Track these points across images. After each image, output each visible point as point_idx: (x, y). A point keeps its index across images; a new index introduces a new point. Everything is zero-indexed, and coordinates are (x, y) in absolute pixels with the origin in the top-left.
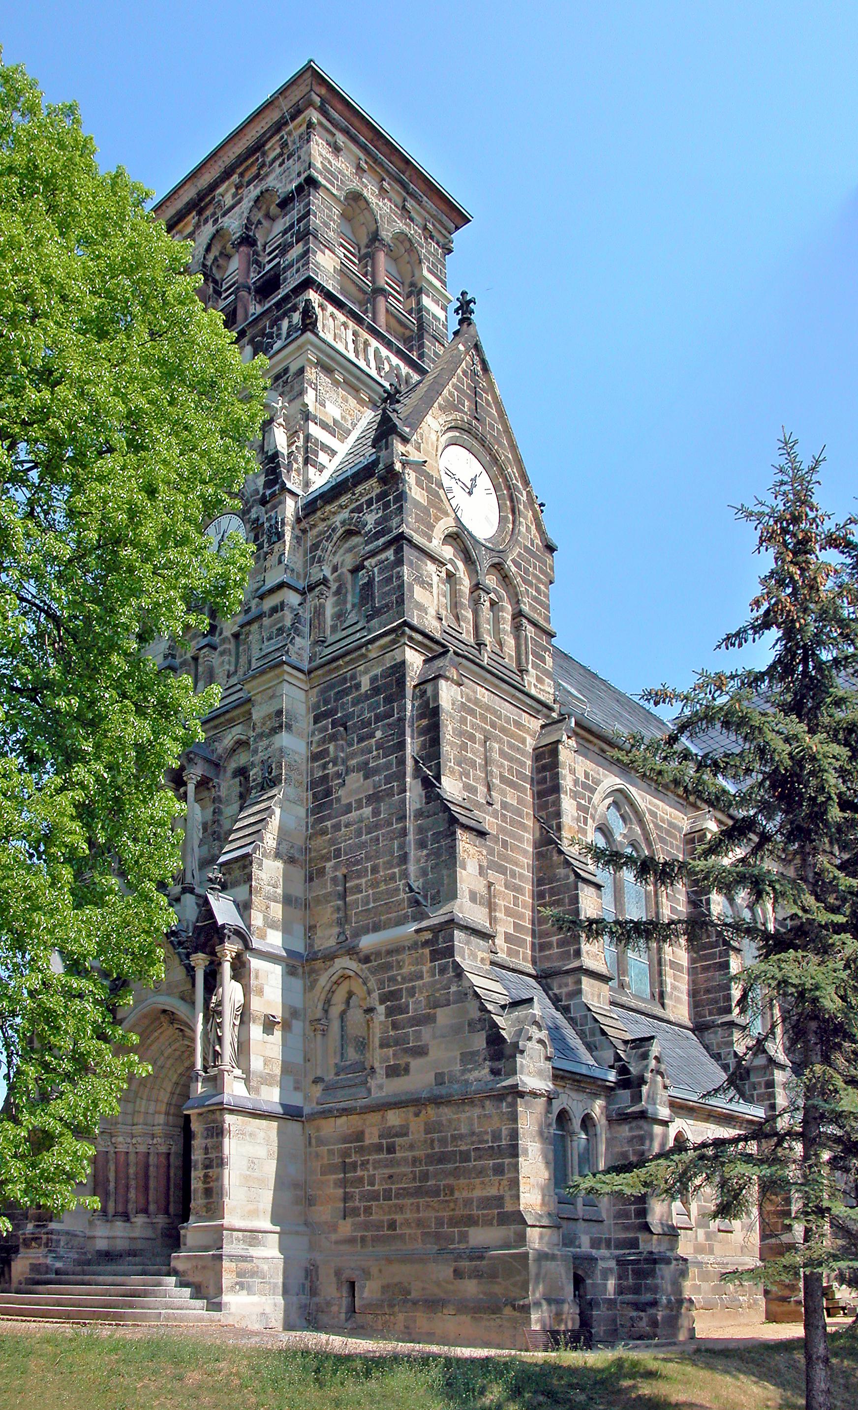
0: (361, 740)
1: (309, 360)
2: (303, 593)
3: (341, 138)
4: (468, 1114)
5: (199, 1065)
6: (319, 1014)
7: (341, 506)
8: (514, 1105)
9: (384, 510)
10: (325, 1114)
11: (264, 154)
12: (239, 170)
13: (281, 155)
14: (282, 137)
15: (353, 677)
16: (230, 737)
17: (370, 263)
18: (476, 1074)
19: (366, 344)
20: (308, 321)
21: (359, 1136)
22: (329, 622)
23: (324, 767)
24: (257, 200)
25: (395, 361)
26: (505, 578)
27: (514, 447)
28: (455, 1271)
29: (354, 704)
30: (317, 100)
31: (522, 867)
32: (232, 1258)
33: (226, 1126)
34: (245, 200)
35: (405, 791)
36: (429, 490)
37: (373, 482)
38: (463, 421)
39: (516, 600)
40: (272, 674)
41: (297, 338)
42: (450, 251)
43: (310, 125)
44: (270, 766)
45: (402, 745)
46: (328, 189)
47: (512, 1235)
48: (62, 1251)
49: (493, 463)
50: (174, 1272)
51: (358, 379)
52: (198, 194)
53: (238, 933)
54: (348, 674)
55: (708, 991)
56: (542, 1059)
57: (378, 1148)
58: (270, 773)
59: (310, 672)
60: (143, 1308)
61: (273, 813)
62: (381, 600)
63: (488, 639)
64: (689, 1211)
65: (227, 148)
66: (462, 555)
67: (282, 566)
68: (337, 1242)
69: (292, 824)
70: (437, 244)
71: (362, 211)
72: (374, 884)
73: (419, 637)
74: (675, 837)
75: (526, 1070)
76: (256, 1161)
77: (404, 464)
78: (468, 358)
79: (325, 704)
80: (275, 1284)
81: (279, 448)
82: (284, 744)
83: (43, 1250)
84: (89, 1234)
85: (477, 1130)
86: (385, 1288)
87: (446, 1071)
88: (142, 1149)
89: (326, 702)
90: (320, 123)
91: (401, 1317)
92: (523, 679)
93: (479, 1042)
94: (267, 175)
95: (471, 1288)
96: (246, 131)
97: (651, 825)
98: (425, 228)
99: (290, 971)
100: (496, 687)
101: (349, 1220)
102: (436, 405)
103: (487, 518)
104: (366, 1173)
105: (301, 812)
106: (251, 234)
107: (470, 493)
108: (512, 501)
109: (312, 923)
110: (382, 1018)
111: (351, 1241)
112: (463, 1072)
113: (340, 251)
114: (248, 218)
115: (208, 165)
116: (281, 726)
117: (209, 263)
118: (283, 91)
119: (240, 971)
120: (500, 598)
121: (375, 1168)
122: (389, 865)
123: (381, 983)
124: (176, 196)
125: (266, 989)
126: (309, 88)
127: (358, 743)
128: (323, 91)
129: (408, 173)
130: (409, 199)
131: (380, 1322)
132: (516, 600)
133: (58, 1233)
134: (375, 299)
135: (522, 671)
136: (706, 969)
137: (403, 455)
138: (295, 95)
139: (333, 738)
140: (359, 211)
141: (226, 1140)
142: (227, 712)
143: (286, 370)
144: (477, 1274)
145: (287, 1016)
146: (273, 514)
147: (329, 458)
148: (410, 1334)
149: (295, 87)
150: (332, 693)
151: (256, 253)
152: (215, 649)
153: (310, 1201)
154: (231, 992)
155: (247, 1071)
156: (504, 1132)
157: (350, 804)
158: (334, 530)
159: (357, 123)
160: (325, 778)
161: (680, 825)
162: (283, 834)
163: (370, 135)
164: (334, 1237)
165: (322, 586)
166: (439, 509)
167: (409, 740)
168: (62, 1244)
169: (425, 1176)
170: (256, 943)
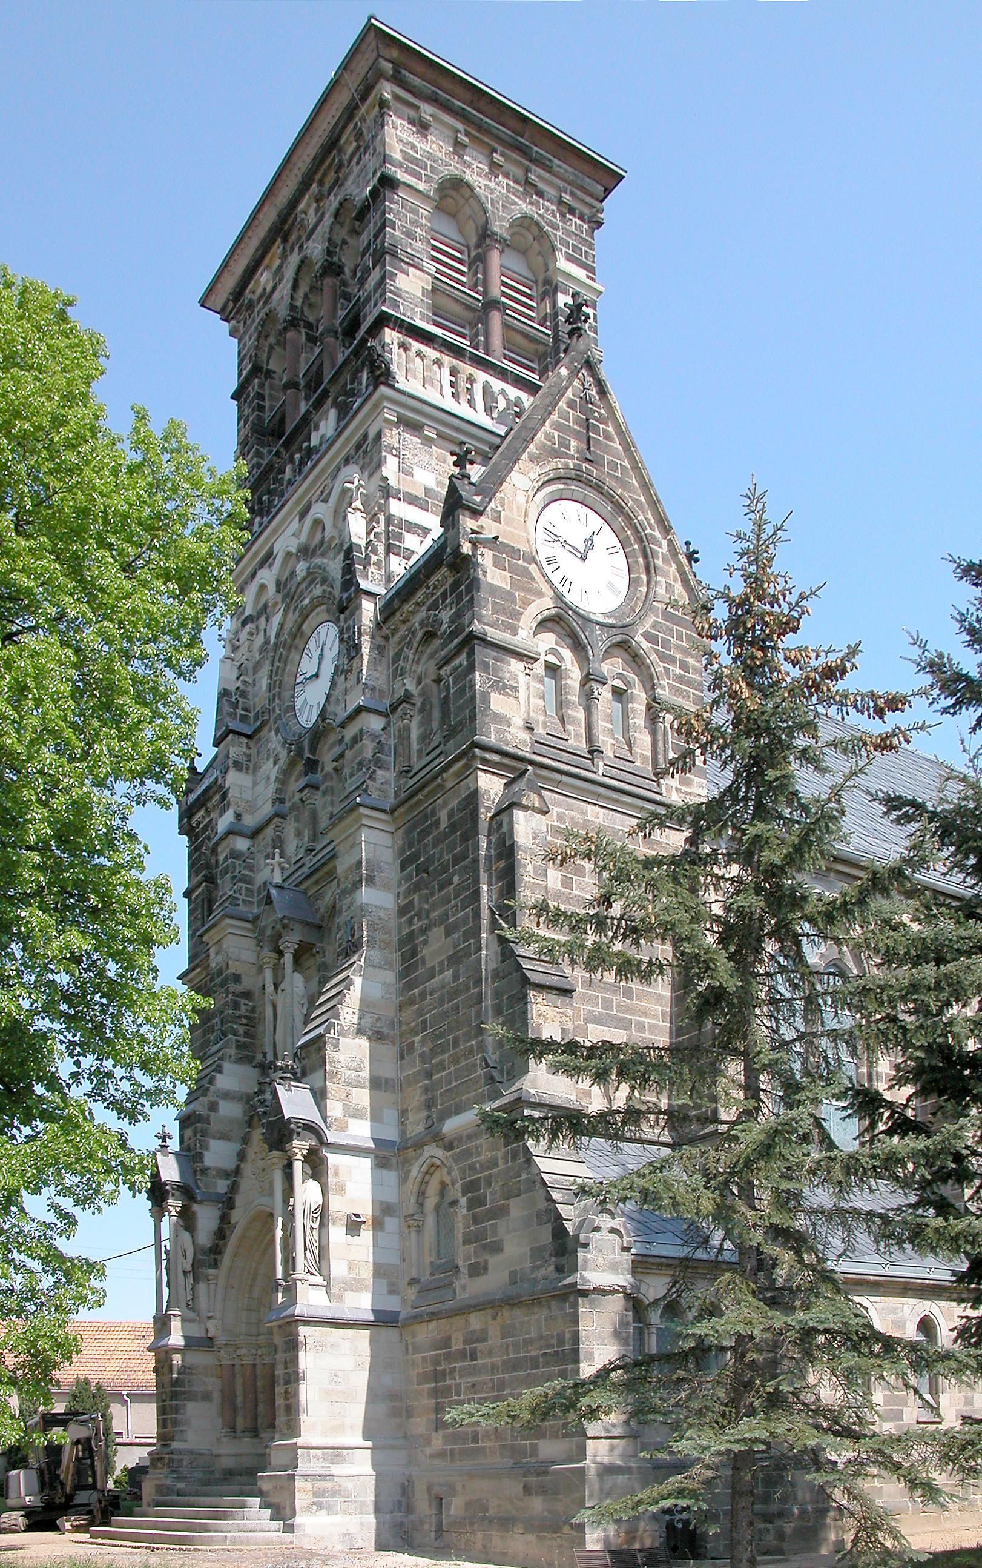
0: (441, 888)
1: (387, 420)
2: (387, 716)
3: (427, 110)
4: (537, 1316)
5: (279, 1276)
6: (412, 1208)
7: (417, 604)
8: (575, 1305)
9: (458, 604)
10: (417, 1319)
11: (341, 151)
12: (317, 177)
13: (358, 148)
14: (356, 124)
15: (433, 813)
16: (330, 893)
17: (481, 269)
18: (543, 1271)
19: (471, 379)
20: (378, 373)
21: (446, 1342)
23: (410, 922)
24: (337, 215)
25: (514, 393)
26: (635, 659)
27: (646, 486)
28: (525, 1487)
29: (434, 847)
30: (388, 67)
31: (655, 1017)
32: (306, 1477)
33: (301, 1338)
34: (327, 216)
35: (480, 949)
36: (514, 569)
37: (444, 570)
38: (567, 467)
39: (650, 685)
40: (349, 819)
41: (370, 395)
42: (599, 224)
43: (383, 104)
44: (352, 928)
45: (477, 893)
46: (409, 186)
47: (574, 1447)
48: (185, 1471)
49: (618, 514)
50: (260, 1493)
51: (458, 430)
52: (279, 216)
53: (310, 1128)
54: (429, 810)
56: (617, 1249)
57: (462, 1355)
58: (353, 936)
59: (393, 811)
60: (216, 1531)
61: (351, 983)
62: (456, 717)
63: (607, 742)
65: (299, 151)
66: (569, 641)
67: (361, 686)
68: (432, 1456)
69: (377, 992)
70: (581, 218)
71: (467, 200)
72: (455, 1060)
73: (496, 758)
75: (591, 1265)
76: (340, 1374)
77: (475, 544)
78: (576, 383)
79: (410, 847)
80: (363, 1503)
81: (354, 540)
82: (364, 901)
83: (166, 1470)
84: (215, 1452)
85: (544, 1334)
86: (468, 1505)
87: (518, 1268)
88: (248, 1360)
89: (410, 846)
90: (396, 97)
91: (480, 1535)
92: (659, 785)
93: (545, 1235)
94: (345, 179)
95: (537, 1505)
96: (316, 124)
99: (381, 1162)
100: (616, 801)
101: (440, 1432)
102: (525, 456)
103: (610, 585)
104: (453, 1381)
105: (390, 976)
106: (335, 259)
107: (583, 559)
108: (645, 557)
109: (405, 1106)
110: (465, 1211)
111: (442, 1454)
112: (534, 1269)
113: (431, 267)
114: (329, 240)
115: (284, 177)
116: (361, 881)
117: (298, 303)
118: (346, 65)
119: (316, 1167)
120: (628, 684)
121: (461, 1377)
122: (468, 1037)
123: (463, 1171)
124: (256, 222)
125: (349, 1187)
126: (375, 54)
127: (439, 891)
128: (395, 53)
129: (527, 134)
130: (533, 167)
131: (463, 1541)
132: (650, 684)
133: (180, 1452)
134: (487, 316)
137: (473, 532)
138: (362, 67)
139: (417, 887)
140: (462, 201)
141: (302, 1354)
142: (324, 864)
143: (365, 436)
144: (543, 1491)
145: (378, 1213)
146: (351, 622)
147: (419, 539)
148: (487, 1553)
149: (359, 56)
150: (415, 834)
151: (344, 283)
152: (318, 788)
153: (409, 1413)
154: (307, 1193)
155: (328, 1279)
156: (568, 1336)
157: (433, 967)
158: (414, 633)
159: (448, 85)
160: (411, 935)
162: (366, 1005)
163: (468, 96)
164: (428, 1451)
165: (404, 705)
166: (529, 590)
167: (485, 888)
168: (185, 1463)
170: (331, 1137)
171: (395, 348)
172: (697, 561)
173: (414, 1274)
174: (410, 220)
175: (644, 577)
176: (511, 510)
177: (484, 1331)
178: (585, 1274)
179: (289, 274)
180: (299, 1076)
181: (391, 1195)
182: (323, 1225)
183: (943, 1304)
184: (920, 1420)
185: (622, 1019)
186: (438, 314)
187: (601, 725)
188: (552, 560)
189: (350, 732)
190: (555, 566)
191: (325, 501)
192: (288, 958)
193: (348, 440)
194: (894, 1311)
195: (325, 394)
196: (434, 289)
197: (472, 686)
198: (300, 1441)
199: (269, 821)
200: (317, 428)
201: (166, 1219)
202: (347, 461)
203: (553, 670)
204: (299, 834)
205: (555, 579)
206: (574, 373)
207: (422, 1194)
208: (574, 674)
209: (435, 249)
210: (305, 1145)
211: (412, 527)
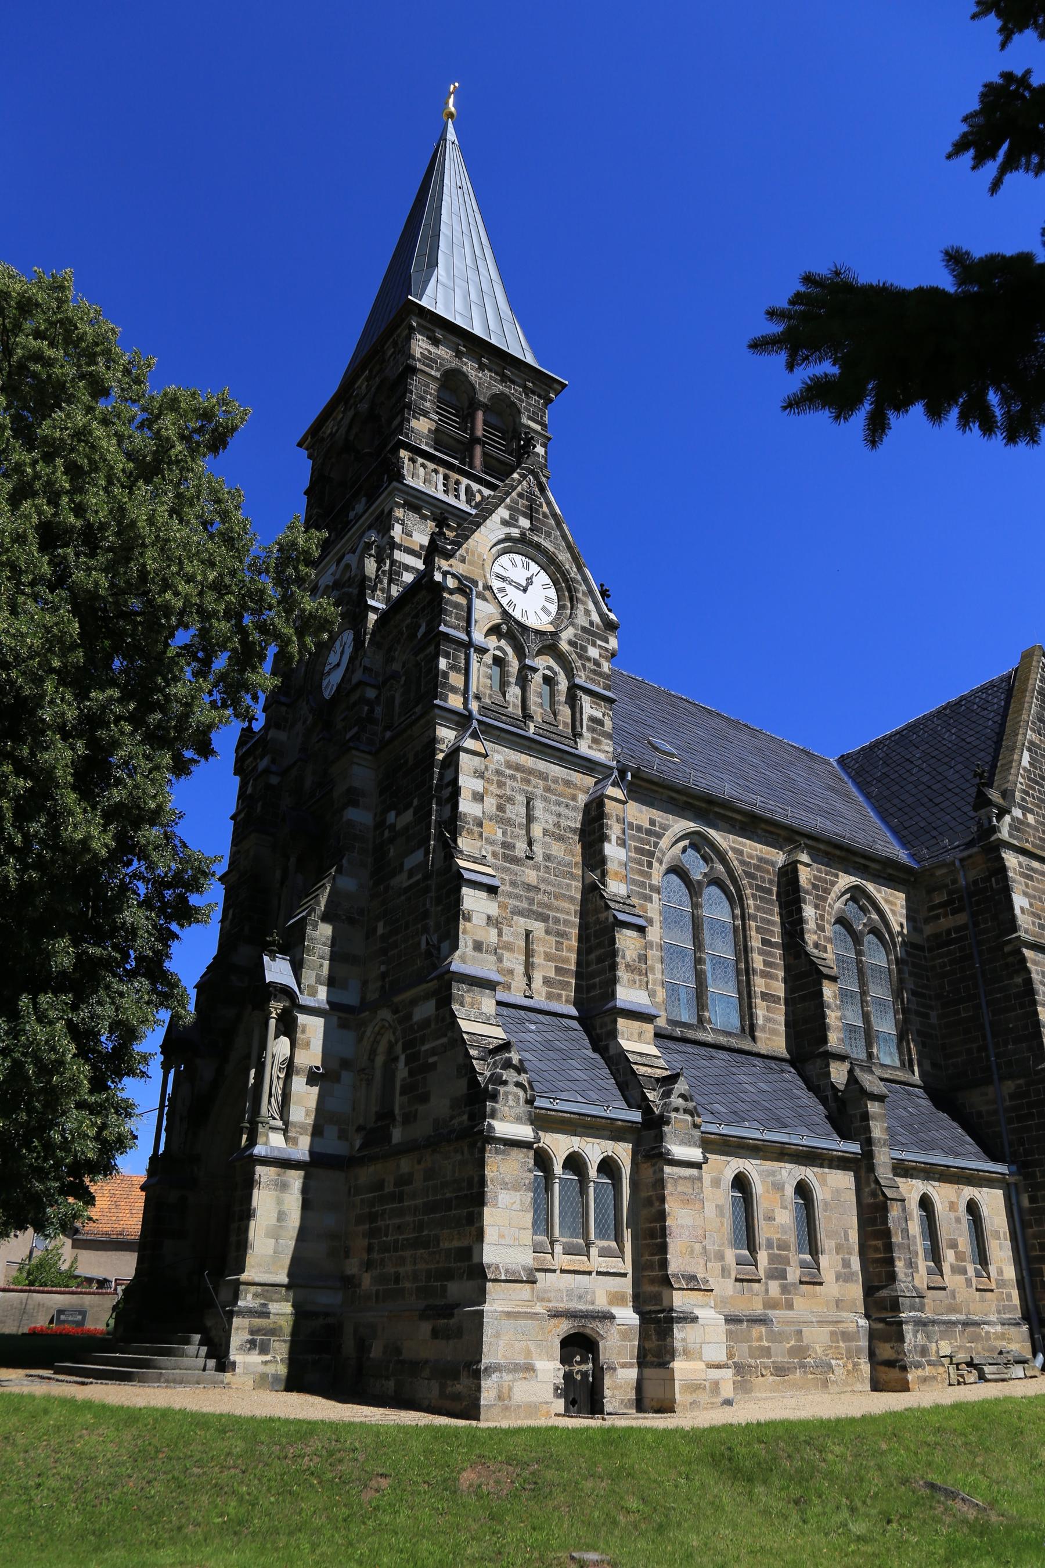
19: (458, 483)
21: (380, 1185)
31: (568, 913)
33: (257, 1177)
39: (570, 675)
53: (285, 992)
63: (534, 709)
74: (768, 872)
92: (576, 743)
97: (736, 863)
98: (525, 387)
117: (351, 438)
120: (555, 673)
141: (255, 1192)
155: (286, 1123)
161: (774, 859)
171: (406, 461)
172: (608, 596)
174: (424, 391)
175: (569, 605)
176: (473, 555)
178: (494, 1122)
179: (346, 422)
183: (816, 1169)
184: (804, 1279)
186: (438, 444)
187: (533, 699)
188: (502, 590)
189: (354, 698)
190: (503, 594)
191: (354, 553)
193: (372, 514)
194: (773, 1173)
196: (437, 430)
198: (244, 1277)
200: (353, 509)
202: (369, 528)
203: (499, 662)
205: (504, 602)
207: (373, 1053)
209: (438, 407)
210: (280, 1005)
211: (407, 568)
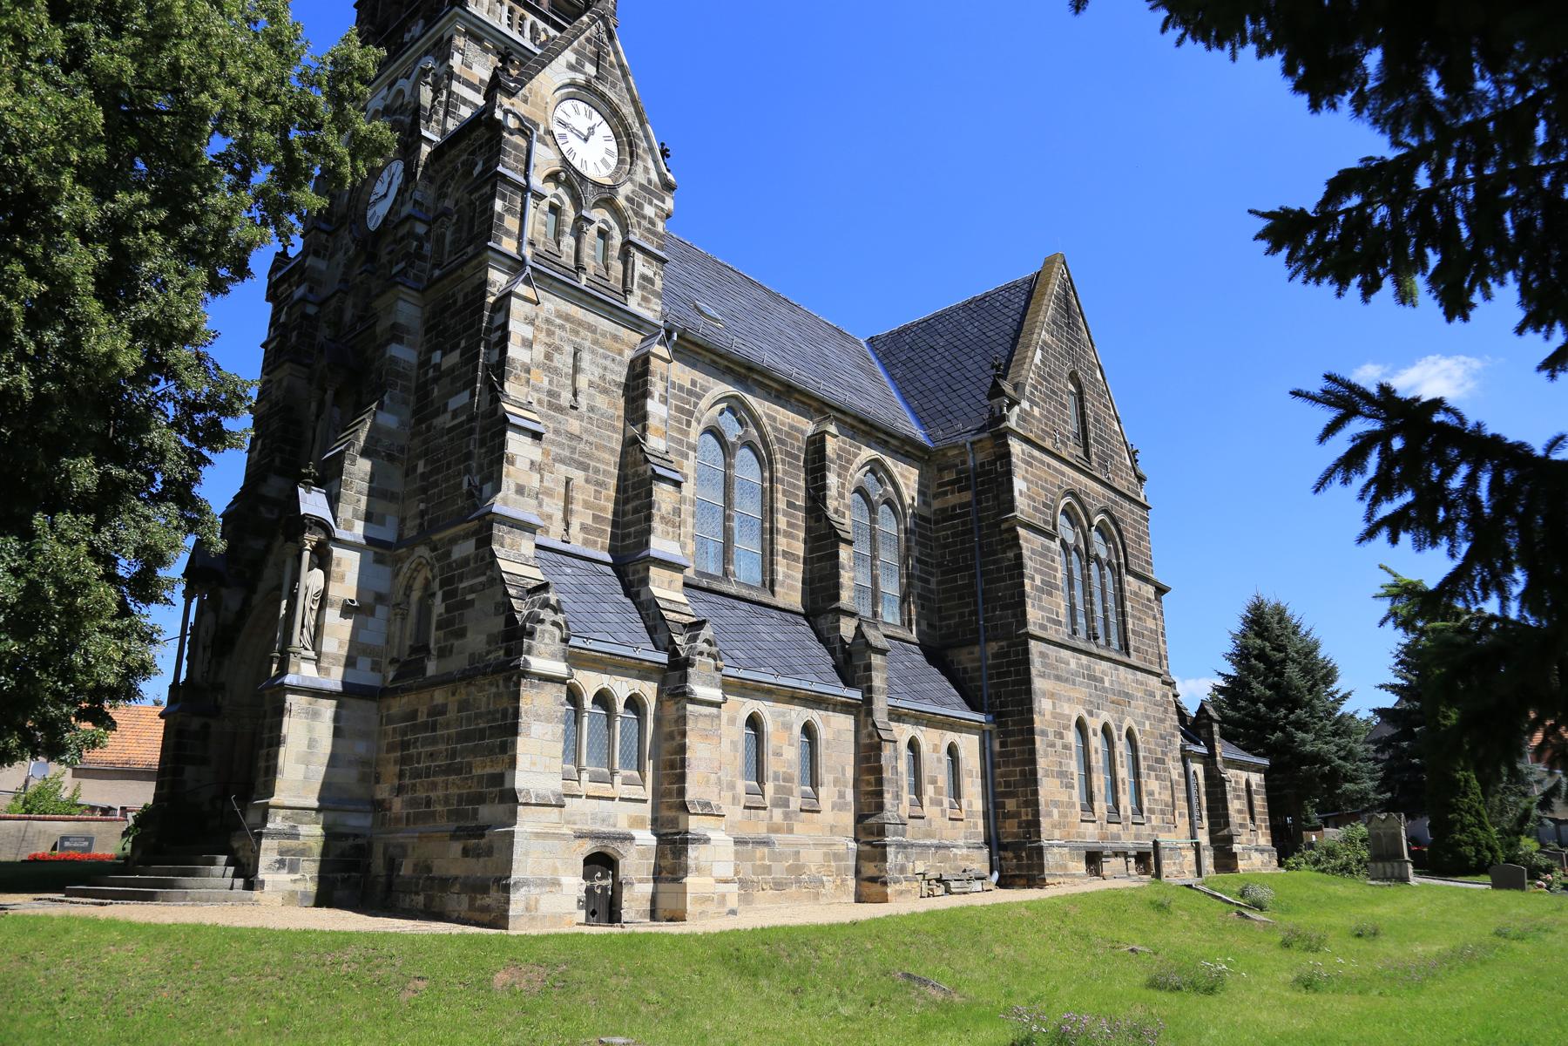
6: (399, 597)
8: (518, 684)
19: (522, 18)
21: (413, 715)
22: (447, 248)
31: (608, 464)
39: (625, 230)
45: (477, 355)
55: (821, 580)
57: (425, 727)
59: (425, 289)
63: (591, 260)
64: (817, 794)
103: (604, 161)
123: (442, 569)
135: (627, 291)
136: (820, 559)
141: (286, 719)
154: (312, 580)
155: (319, 654)
169: (453, 754)
173: (395, 654)
177: (445, 706)
180: (320, 483)
181: (383, 586)
182: (322, 608)
185: (581, 463)
187: (587, 251)
188: (563, 136)
192: (330, 394)
194: (783, 714)
195: (417, 10)
197: (492, 208)
198: (272, 801)
199: (334, 294)
201: (195, 600)
202: (426, 53)
204: (355, 306)
205: (565, 149)
206: (594, 21)
207: (409, 588)
208: (570, 215)
210: (315, 538)
211: (465, 102)
